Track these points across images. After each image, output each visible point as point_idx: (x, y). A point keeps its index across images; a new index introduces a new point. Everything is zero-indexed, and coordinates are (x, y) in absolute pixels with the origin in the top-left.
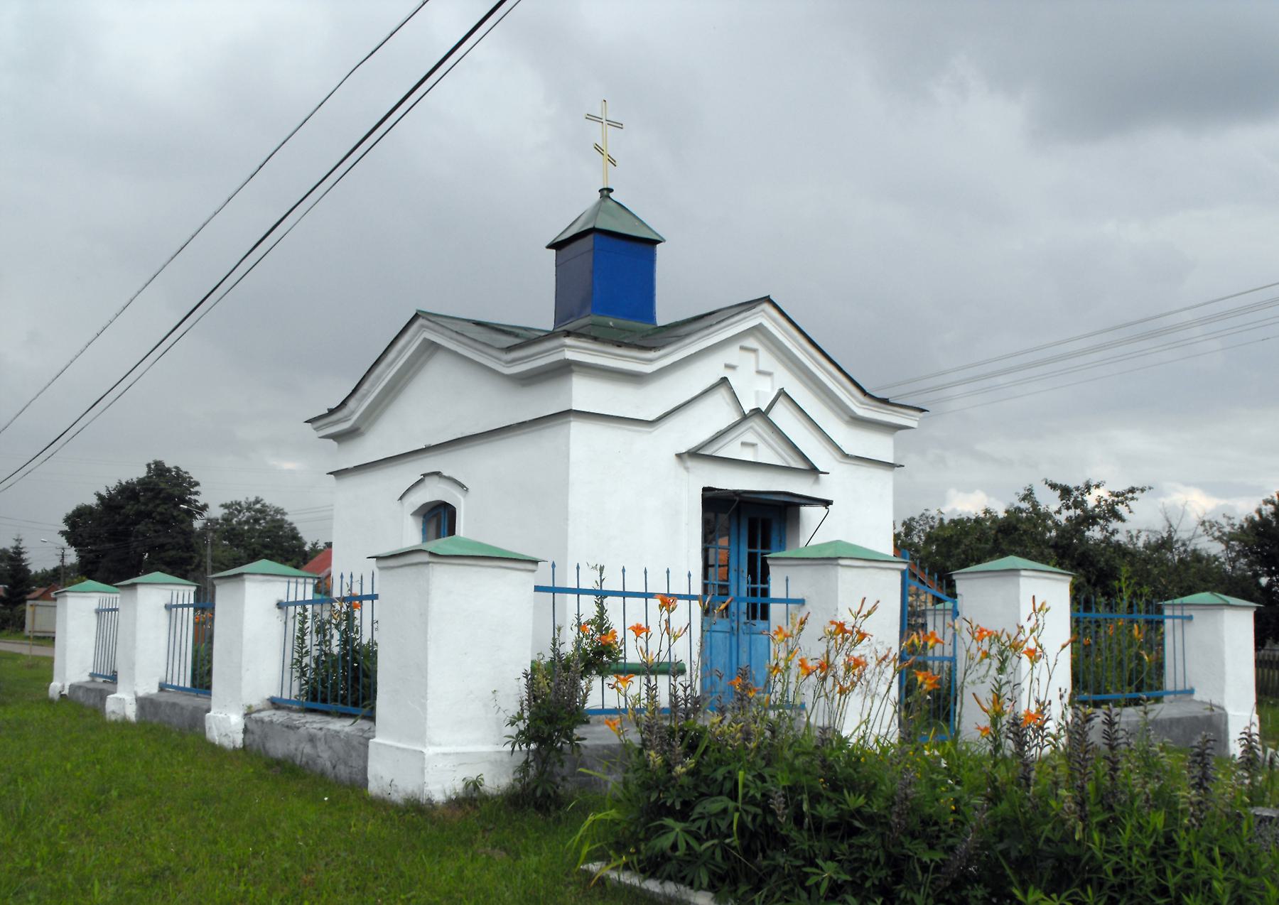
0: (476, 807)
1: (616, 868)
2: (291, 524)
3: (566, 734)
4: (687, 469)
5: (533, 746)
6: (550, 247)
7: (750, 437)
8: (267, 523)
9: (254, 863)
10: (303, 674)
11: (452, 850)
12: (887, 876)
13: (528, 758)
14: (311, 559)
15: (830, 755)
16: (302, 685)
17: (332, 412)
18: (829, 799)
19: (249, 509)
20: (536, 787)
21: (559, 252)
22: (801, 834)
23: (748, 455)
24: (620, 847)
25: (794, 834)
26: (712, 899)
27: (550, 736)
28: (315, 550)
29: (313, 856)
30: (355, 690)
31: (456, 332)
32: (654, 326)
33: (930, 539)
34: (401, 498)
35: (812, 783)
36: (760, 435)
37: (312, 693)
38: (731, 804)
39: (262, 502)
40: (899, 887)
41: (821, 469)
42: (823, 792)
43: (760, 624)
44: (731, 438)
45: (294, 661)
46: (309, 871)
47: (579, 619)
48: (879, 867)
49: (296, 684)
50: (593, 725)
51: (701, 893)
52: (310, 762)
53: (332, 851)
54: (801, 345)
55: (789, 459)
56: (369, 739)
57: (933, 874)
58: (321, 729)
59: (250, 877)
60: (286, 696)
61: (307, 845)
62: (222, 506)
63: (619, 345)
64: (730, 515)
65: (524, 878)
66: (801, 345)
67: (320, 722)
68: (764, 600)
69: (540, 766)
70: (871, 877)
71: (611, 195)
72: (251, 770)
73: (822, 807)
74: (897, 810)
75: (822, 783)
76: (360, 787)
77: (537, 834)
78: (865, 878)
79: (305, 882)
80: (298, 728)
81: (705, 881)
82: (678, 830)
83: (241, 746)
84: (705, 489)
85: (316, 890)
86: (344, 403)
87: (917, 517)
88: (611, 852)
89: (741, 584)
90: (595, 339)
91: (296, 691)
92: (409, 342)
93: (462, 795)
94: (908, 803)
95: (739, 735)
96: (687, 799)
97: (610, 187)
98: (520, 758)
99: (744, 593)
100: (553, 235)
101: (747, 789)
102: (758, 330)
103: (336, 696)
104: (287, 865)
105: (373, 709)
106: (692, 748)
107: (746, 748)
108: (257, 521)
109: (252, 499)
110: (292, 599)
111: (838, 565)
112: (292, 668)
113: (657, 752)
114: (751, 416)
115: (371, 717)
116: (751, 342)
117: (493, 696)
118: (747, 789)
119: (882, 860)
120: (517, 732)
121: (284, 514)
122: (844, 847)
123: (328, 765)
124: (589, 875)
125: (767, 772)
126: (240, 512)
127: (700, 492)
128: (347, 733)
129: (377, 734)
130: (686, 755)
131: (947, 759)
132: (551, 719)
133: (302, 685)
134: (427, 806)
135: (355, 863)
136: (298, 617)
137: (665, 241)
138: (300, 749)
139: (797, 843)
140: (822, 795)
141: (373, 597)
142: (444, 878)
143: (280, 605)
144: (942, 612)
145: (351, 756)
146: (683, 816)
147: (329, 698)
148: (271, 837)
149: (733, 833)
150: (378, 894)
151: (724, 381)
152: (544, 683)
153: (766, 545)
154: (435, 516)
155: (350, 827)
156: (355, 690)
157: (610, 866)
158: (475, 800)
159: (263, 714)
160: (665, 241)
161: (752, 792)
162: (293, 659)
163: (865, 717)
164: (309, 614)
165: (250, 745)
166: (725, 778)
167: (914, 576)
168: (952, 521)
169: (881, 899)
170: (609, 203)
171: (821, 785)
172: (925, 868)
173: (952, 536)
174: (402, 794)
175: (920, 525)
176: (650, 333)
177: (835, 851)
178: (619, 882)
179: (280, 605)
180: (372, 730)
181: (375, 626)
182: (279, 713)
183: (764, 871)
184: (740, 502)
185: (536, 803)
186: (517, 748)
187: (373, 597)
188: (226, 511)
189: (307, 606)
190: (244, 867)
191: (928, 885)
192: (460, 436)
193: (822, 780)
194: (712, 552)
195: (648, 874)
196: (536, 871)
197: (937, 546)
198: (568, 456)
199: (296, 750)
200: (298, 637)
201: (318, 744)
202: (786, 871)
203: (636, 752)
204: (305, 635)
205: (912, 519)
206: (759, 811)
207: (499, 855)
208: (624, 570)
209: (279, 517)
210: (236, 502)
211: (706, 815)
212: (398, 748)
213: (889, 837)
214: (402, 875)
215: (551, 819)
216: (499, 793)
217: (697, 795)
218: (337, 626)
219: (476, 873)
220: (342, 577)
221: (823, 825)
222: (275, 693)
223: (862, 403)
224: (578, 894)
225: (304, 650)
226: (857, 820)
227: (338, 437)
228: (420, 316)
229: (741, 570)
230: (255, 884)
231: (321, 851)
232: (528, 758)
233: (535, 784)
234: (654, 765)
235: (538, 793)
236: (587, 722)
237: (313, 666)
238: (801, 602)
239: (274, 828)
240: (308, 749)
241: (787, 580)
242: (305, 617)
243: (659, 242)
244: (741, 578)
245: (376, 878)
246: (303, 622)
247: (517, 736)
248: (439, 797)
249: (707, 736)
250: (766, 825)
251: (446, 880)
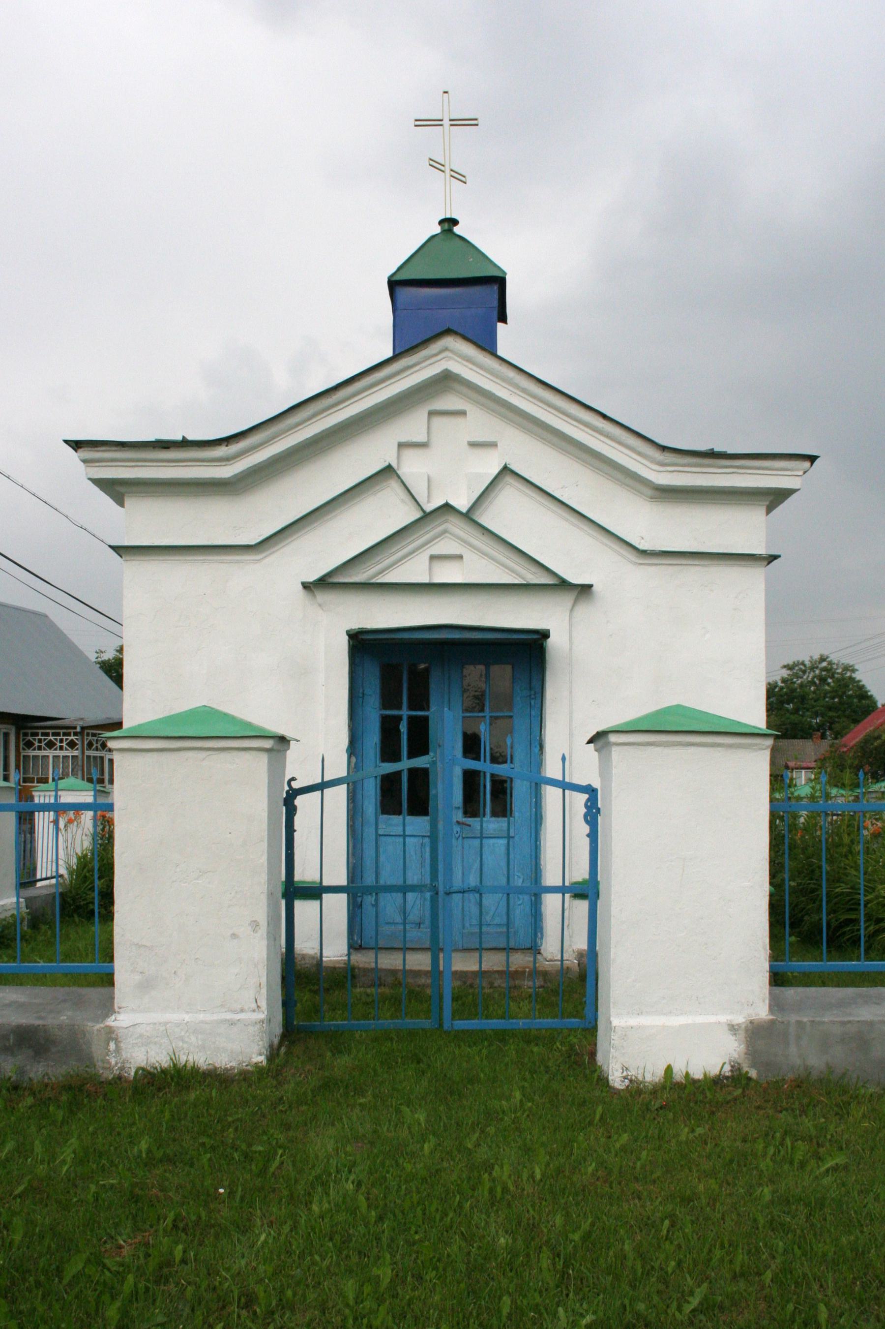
2: (859, 681)
19: (813, 668)
44: (405, 551)
54: (524, 390)
55: (523, 572)
62: (785, 667)
71: (457, 230)
109: (816, 657)
121: (854, 671)
126: (804, 672)
188: (789, 672)
210: (798, 662)
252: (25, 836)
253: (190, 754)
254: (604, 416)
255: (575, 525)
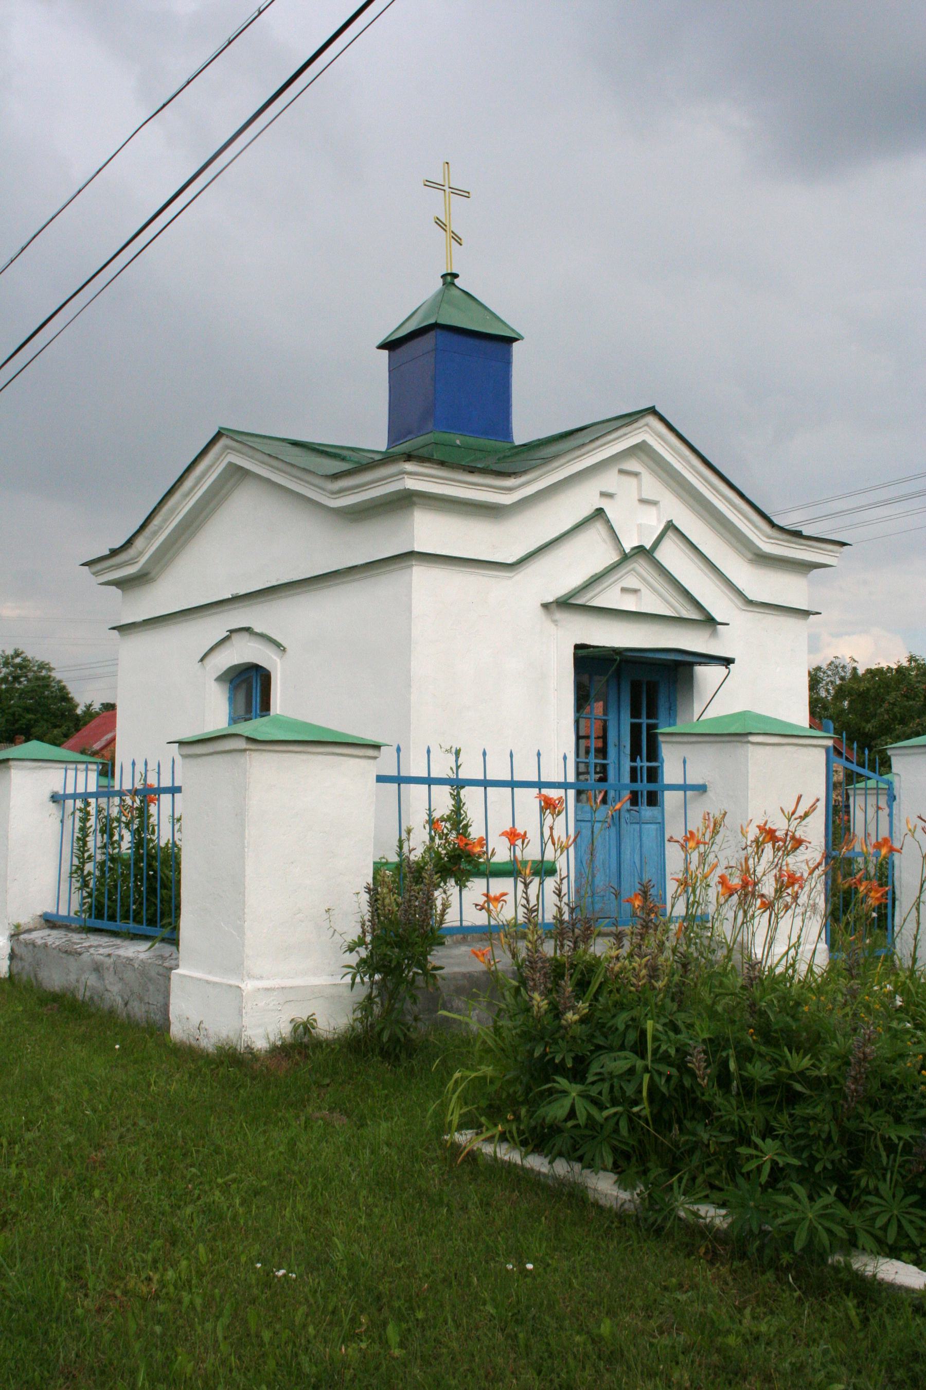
0: (307, 1057)
1: (490, 1140)
2: (60, 682)
3: (419, 961)
4: (555, 622)
5: (377, 977)
6: (382, 347)
7: (631, 581)
8: (29, 680)
9: (29, 1136)
10: (85, 884)
11: (280, 1114)
12: (843, 1157)
13: (371, 993)
14: (85, 724)
15: (761, 999)
16: (84, 898)
17: (114, 553)
18: (761, 1055)
20: (382, 1030)
21: (392, 353)
22: (729, 1101)
23: (629, 604)
24: (494, 1112)
25: (719, 1100)
26: (615, 1183)
27: (399, 964)
28: (89, 714)
29: (103, 1126)
30: (151, 904)
31: (269, 455)
32: (509, 445)
33: (841, 693)
34: (202, 660)
35: (738, 1035)
36: (644, 580)
37: (96, 907)
38: (639, 1063)
39: (23, 655)
40: (859, 1172)
41: (719, 619)
42: (754, 1046)
43: (647, 812)
45: (74, 868)
46: (98, 1147)
47: (430, 815)
48: (831, 1146)
49: (76, 898)
50: (450, 947)
51: (601, 1174)
52: (96, 998)
53: (127, 1118)
54: (693, 467)
56: (171, 969)
57: (901, 1156)
58: (109, 955)
59: (23, 1155)
60: (63, 912)
61: (94, 1110)
63: (472, 470)
64: (607, 681)
65: (372, 1152)
66: (693, 467)
67: (109, 946)
68: (652, 787)
69: (386, 1003)
70: (821, 1159)
71: (457, 281)
72: (21, 1008)
73: (754, 1066)
74: (853, 1073)
75: (752, 1035)
76: (159, 1029)
77: (386, 1092)
78: (813, 1160)
79: (95, 1162)
80: (80, 954)
81: (609, 1161)
82: (574, 1094)
83: (7, 976)
84: (578, 647)
85: (109, 1173)
86: (129, 542)
87: (824, 667)
88: (483, 1120)
89: (622, 762)
90: (442, 464)
91: (75, 906)
92: (210, 467)
93: (289, 1040)
94: (867, 1065)
95: (644, 972)
96: (580, 1054)
97: (454, 271)
98: (362, 992)
99: (626, 778)
100: (384, 333)
101: (657, 1044)
102: (642, 449)
103: (128, 911)
104: (71, 1139)
105: (176, 929)
106: (582, 985)
107: (654, 988)
108: (16, 679)
110: (70, 790)
111: (749, 742)
112: (71, 877)
113: (541, 994)
114: (631, 556)
115: (173, 940)
116: (632, 465)
117: (326, 916)
118: (657, 1044)
119: (835, 1138)
120: (358, 959)
121: (50, 669)
122: (784, 1118)
123: (119, 1000)
124: (456, 1148)
125: (681, 1019)
127: (571, 650)
128: (142, 961)
129: (181, 963)
130: (578, 998)
131: (901, 995)
132: (401, 943)
133: (84, 898)
134: (246, 1055)
135: (158, 1135)
136: (78, 814)
137: (522, 338)
138: (83, 979)
139: (723, 1113)
140: (753, 1051)
141: (174, 790)
142: (271, 1153)
143: (56, 798)
144: (863, 792)
145: (148, 991)
146: (578, 1074)
147: (118, 915)
148: (48, 1099)
149: (642, 1099)
150: (188, 1177)
151: (599, 513)
152: (390, 900)
153: (652, 713)
154: (243, 681)
155: (149, 1085)
156: (151, 904)
157: (483, 1137)
158: (306, 1047)
159: (35, 935)
160: (522, 338)
161: (664, 1047)
162: (72, 865)
163: (794, 940)
164: (92, 809)
165: (18, 974)
166: (627, 1027)
167: (840, 754)
168: (869, 671)
169: (835, 1188)
170: (454, 291)
171: (750, 1038)
172: (890, 1147)
173: (868, 689)
174: (213, 1040)
175: (828, 676)
176: (507, 454)
177: (774, 1124)
178: (495, 1158)
179: (56, 798)
180: (174, 956)
181: (177, 827)
182: (55, 933)
183: (682, 1150)
184: (621, 661)
185: (382, 1049)
186: (358, 979)
187: (174, 790)
189: (90, 800)
190: (15, 1143)
191: (896, 1169)
192: (275, 583)
193: (752, 1030)
194: (582, 722)
195: (530, 1148)
196: (389, 1144)
197: (851, 703)
198: (410, 611)
199: (78, 981)
200: (79, 839)
201: (106, 976)
202: (712, 1150)
203: (513, 991)
204: (87, 836)
205: (819, 669)
206: (674, 1071)
207: (339, 1121)
208: (484, 754)
209: (44, 673)
211: (606, 1075)
212: (208, 982)
213: (842, 1106)
214: (217, 1151)
215: (400, 1071)
216: (336, 1036)
217: (592, 1048)
218: (127, 825)
219: (312, 1146)
220: (134, 764)
221: (756, 1089)
222: (50, 908)
223: (769, 537)
224: (442, 1174)
225: (86, 855)
226: (798, 1082)
227: (118, 583)
228: (223, 434)
229: (622, 744)
230: (30, 1165)
231: (114, 1119)
232: (371, 993)
233: (381, 1026)
234: (538, 1012)
235: (385, 1038)
236: (443, 944)
237: (97, 873)
238: (702, 789)
239: (52, 1089)
240: (92, 979)
241: (684, 762)
242: (88, 813)
243: (516, 340)
244: (622, 754)
245: (185, 1155)
246: (85, 820)
247: (358, 965)
248: (261, 1044)
249: (601, 972)
250: (682, 1087)
251: (273, 1156)
252: (95, 840)
253: (788, 748)
254: (742, 496)
255: (706, 574)
